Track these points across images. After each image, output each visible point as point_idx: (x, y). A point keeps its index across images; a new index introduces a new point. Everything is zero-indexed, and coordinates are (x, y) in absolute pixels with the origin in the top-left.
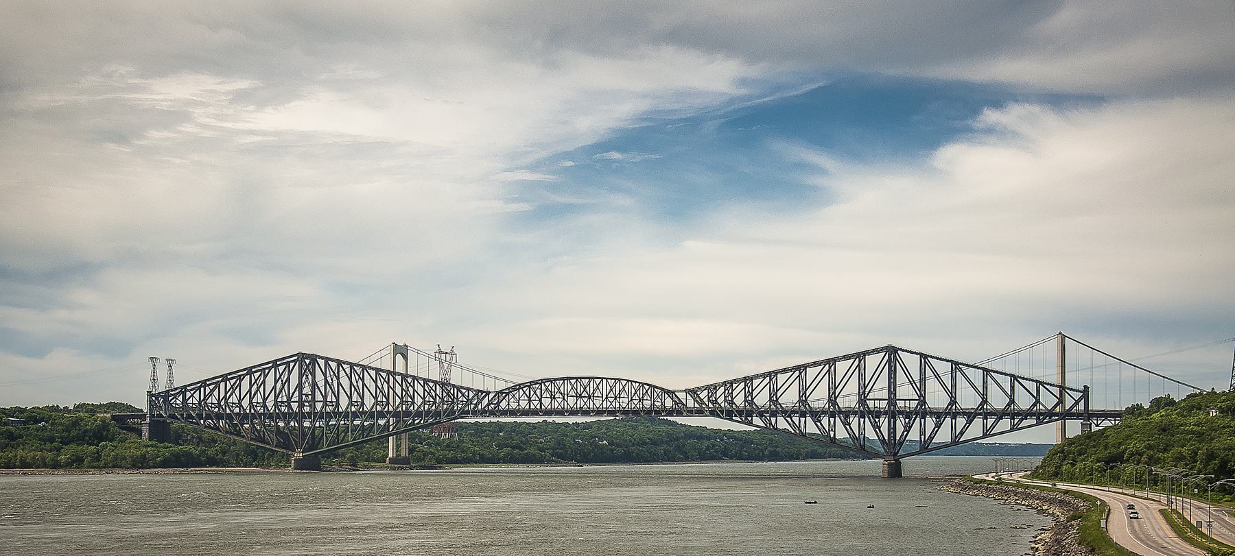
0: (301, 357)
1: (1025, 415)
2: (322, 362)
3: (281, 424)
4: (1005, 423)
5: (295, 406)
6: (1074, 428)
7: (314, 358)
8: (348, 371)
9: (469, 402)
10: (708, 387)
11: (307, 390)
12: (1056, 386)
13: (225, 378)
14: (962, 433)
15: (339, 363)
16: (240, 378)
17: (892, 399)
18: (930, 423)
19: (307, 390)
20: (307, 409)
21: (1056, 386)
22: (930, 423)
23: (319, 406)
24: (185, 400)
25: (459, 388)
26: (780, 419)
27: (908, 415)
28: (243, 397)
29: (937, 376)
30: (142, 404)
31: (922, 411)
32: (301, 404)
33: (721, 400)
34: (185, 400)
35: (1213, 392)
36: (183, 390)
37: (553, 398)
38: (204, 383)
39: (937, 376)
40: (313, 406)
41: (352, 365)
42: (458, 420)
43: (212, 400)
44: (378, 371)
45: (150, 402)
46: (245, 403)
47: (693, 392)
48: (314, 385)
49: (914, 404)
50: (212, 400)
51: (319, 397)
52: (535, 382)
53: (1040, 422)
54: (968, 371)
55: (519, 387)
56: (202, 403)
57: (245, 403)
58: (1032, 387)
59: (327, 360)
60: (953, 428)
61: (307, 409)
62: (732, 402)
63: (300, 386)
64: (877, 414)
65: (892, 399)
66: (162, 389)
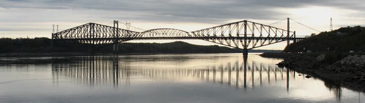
0: (91, 24)
1: (273, 39)
2: (96, 25)
3: (86, 42)
4: (267, 42)
5: (89, 37)
6: (291, 42)
7: (94, 24)
8: (268, 30)
9: (134, 35)
10: (197, 31)
11: (92, 33)
12: (245, 32)
13: (71, 29)
14: (255, 44)
15: (100, 25)
16: (75, 30)
17: (245, 35)
18: (255, 41)
19: (92, 33)
20: (92, 37)
21: (245, 32)
22: (255, 41)
23: (95, 37)
24: (61, 36)
25: (131, 32)
26: (224, 40)
27: (250, 38)
28: (75, 35)
29: (257, 28)
30: (50, 37)
31: (253, 38)
32: (91, 36)
33: (201, 35)
34: (61, 36)
35: (326, 32)
36: (61, 33)
37: (156, 34)
38: (66, 31)
39: (257, 28)
40: (93, 37)
41: (104, 26)
42: (128, 42)
43: (68, 35)
44: (110, 27)
45: (52, 35)
46: (76, 36)
47: (193, 32)
48: (94, 31)
49: (251, 36)
50: (68, 35)
51: (95, 34)
52: (152, 30)
53: (283, 40)
54: (265, 27)
55: (147, 31)
56: (66, 36)
57: (76, 36)
58: (281, 31)
59: (97, 25)
60: (253, 43)
61: (86, 37)
62: (204, 35)
63: (90, 31)
64: (241, 38)
65: (245, 35)
66: (56, 33)
